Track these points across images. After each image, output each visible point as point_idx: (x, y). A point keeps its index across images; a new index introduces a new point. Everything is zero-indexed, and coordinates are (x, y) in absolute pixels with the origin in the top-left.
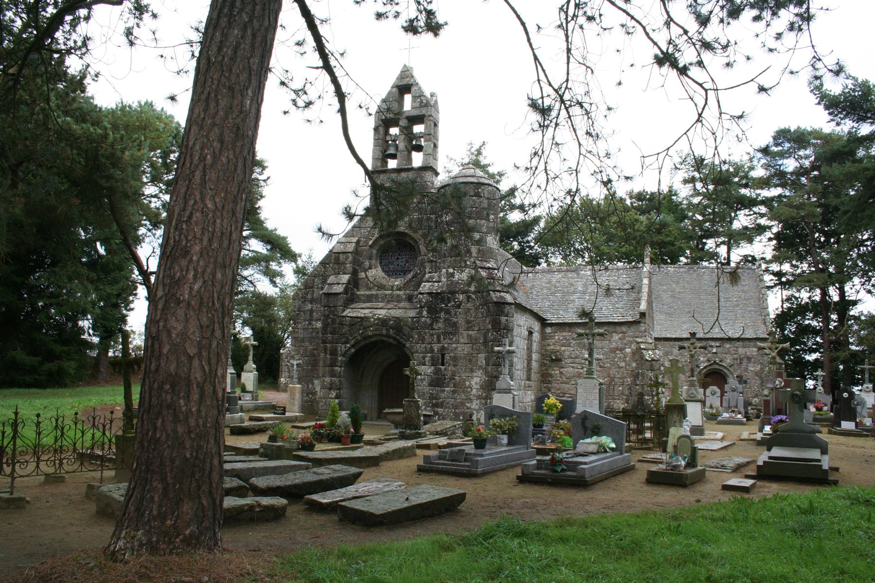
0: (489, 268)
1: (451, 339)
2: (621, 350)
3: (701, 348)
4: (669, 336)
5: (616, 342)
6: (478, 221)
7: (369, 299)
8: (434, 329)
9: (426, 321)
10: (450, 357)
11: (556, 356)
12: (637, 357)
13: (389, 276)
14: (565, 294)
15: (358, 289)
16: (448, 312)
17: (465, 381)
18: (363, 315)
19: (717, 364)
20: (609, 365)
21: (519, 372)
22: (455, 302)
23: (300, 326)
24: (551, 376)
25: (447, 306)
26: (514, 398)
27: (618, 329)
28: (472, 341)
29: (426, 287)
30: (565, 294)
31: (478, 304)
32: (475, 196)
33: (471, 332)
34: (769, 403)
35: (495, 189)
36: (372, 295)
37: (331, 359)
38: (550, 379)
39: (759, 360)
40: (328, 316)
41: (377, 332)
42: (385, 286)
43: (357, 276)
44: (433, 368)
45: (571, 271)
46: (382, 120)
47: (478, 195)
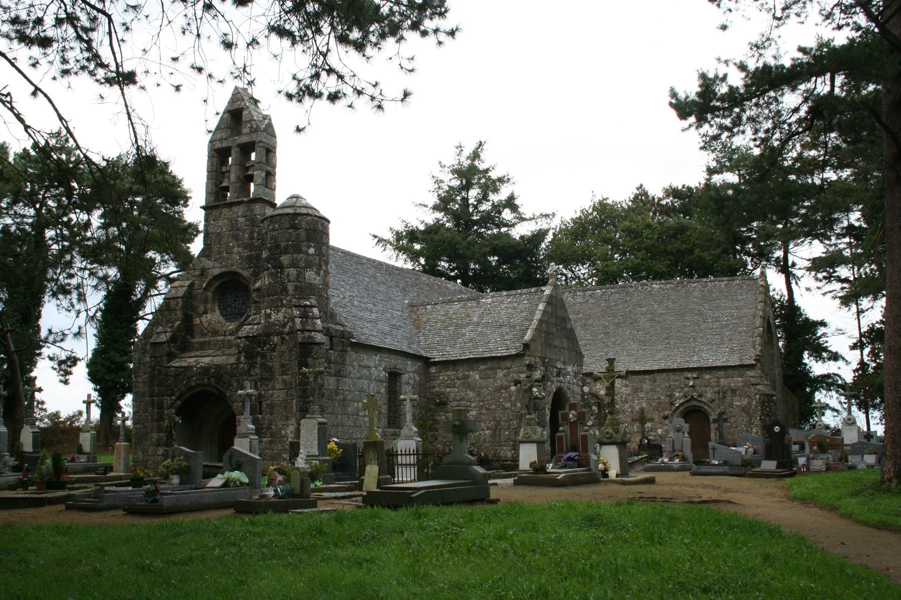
0: (306, 306)
1: (267, 386)
2: (507, 388)
4: (637, 368)
6: (295, 255)
7: (203, 346)
8: (252, 376)
9: (243, 367)
11: (440, 399)
13: (227, 320)
14: (459, 326)
15: (193, 337)
16: (264, 356)
18: (186, 365)
19: (696, 400)
20: (494, 407)
22: (270, 345)
23: (140, 379)
26: (250, 442)
28: (287, 386)
30: (459, 326)
32: (291, 228)
33: (285, 377)
34: (562, 441)
35: (316, 219)
38: (437, 426)
39: (746, 393)
40: (155, 367)
41: (200, 382)
42: (218, 332)
43: (191, 321)
45: (471, 300)
46: (216, 150)
47: (295, 227)
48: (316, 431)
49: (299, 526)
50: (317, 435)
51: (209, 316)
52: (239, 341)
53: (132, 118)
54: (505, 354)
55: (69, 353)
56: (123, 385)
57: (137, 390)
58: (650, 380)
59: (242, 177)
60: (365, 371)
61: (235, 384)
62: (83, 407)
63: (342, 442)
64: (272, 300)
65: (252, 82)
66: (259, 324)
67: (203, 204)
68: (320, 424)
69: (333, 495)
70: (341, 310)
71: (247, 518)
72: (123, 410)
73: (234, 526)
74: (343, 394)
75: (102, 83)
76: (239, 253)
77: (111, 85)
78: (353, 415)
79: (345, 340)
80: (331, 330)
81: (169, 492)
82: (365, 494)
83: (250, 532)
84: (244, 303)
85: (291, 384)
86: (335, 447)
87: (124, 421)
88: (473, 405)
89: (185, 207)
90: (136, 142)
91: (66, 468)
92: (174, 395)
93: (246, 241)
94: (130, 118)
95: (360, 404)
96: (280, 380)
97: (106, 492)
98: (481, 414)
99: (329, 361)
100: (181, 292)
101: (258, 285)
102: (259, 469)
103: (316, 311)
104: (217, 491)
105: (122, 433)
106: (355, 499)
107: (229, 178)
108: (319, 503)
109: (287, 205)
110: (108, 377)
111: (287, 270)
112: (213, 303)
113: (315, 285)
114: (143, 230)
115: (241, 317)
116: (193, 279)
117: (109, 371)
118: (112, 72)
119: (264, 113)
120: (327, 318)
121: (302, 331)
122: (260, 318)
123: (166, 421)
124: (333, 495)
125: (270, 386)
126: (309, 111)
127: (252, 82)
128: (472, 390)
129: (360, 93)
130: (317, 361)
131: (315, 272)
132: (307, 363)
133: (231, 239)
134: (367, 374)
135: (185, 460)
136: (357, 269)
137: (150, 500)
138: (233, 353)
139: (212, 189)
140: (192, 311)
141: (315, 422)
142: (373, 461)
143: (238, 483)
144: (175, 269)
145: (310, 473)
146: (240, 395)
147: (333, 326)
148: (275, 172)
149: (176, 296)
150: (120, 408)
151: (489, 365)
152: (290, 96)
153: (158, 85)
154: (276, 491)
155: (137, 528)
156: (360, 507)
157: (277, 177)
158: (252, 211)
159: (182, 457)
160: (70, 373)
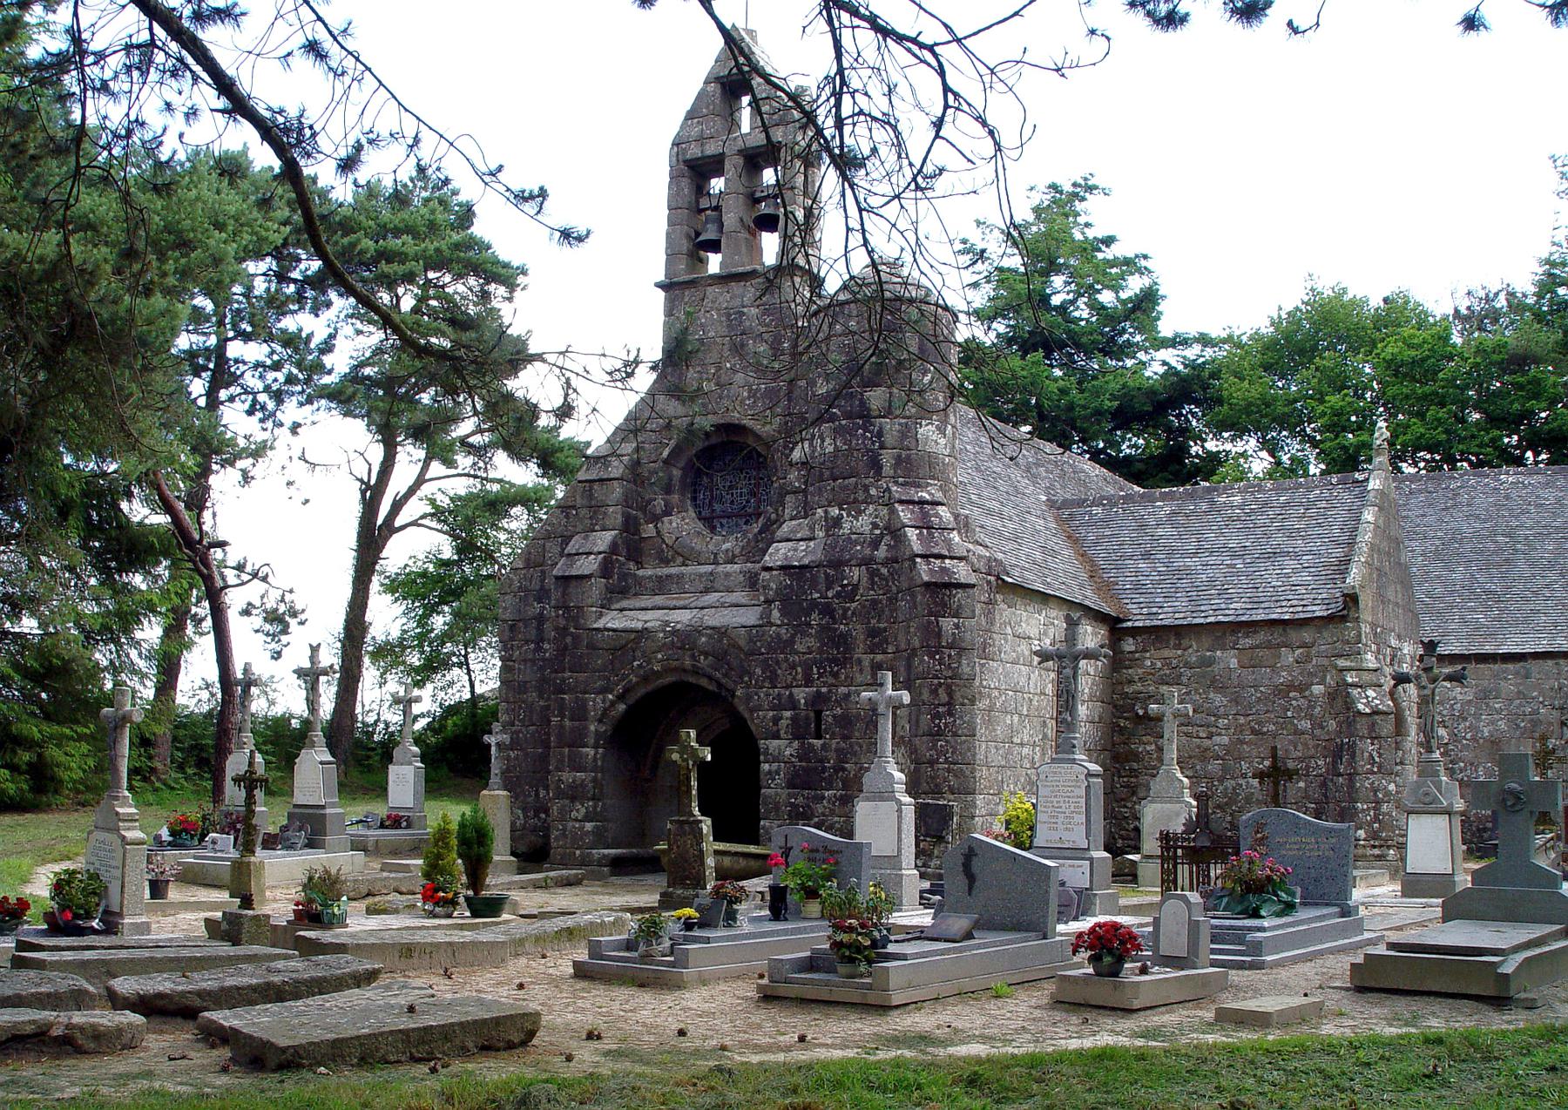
0: (922, 502)
1: (836, 675)
2: (1302, 688)
3: (1449, 678)
5: (1288, 668)
7: (661, 586)
8: (797, 653)
9: (778, 635)
12: (1339, 703)
18: (640, 625)
20: (1272, 727)
21: (1025, 751)
24: (1136, 756)
27: (1294, 636)
29: (779, 553)
38: (1135, 766)
40: (565, 629)
43: (637, 532)
44: (796, 744)
54: (1302, 616)
58: (1517, 674)
61: (758, 671)
64: (844, 488)
67: (661, 277)
74: (989, 696)
88: (1222, 722)
96: (866, 663)
98: (1242, 742)
128: (1221, 689)
151: (1262, 636)
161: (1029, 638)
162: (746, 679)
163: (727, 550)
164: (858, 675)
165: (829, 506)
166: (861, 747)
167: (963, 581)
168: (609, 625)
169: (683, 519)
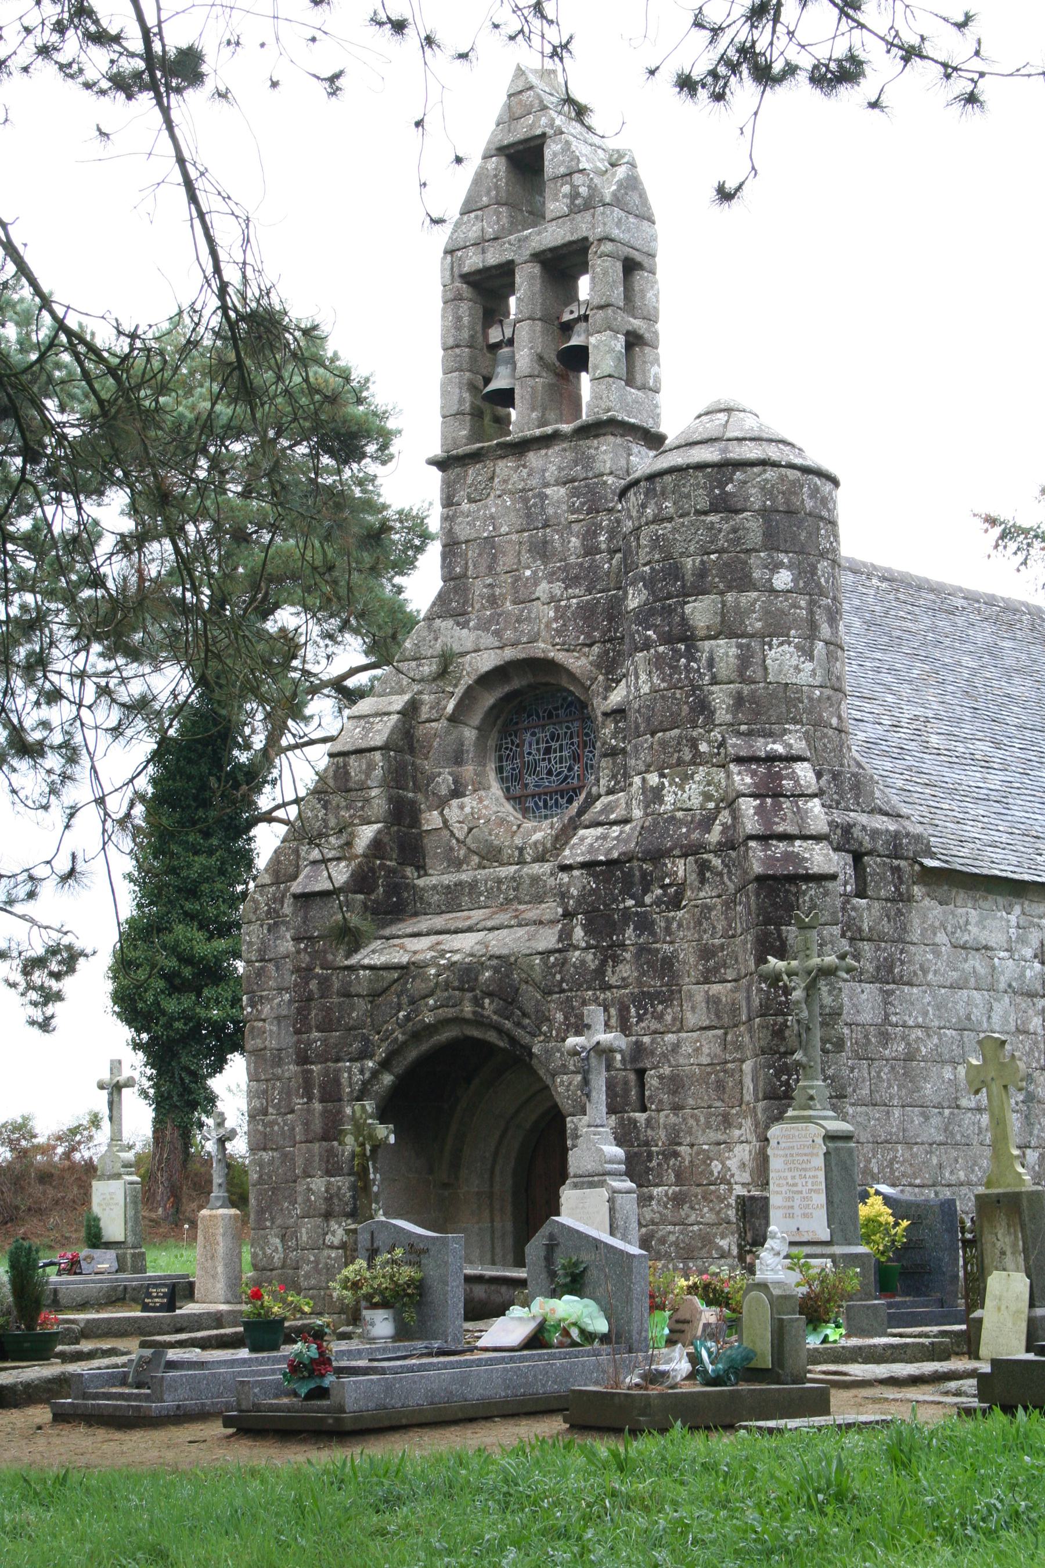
0: (772, 758)
1: (660, 1017)
6: (730, 597)
8: (610, 987)
9: (583, 962)
10: (661, 1077)
13: (525, 812)
15: (422, 869)
16: (645, 924)
17: (708, 1159)
18: (405, 959)
22: (664, 887)
23: (266, 1010)
25: (640, 903)
26: (611, 1201)
31: (731, 886)
32: (714, 509)
33: (716, 989)
35: (796, 474)
36: (459, 884)
37: (325, 1113)
40: (309, 969)
41: (450, 1012)
43: (416, 822)
46: (466, 278)
47: (724, 506)
48: (820, 1162)
49: (772, 1476)
50: (821, 1175)
51: (469, 802)
52: (565, 877)
53: (201, 196)
55: (55, 935)
56: (217, 1028)
57: (258, 1043)
59: (552, 357)
60: (975, 963)
61: (559, 1016)
62: (100, 1101)
63: (909, 1195)
64: (663, 744)
65: (565, 46)
66: (626, 821)
67: (436, 450)
68: (830, 1137)
69: (882, 1370)
70: (888, 765)
71: (603, 1447)
72: (220, 1106)
73: (564, 1474)
75: (103, 92)
76: (553, 599)
77: (130, 97)
78: (940, 1106)
79: (903, 863)
80: (856, 832)
81: (362, 1363)
82: (986, 1368)
83: (614, 1494)
84: (576, 758)
85: (734, 1011)
86: (886, 1215)
87: (222, 1142)
89: (384, 463)
90: (217, 270)
91: (55, 1292)
92: (371, 1057)
93: (572, 560)
94: (193, 198)
95: (962, 1070)
96: (699, 998)
97: (172, 1365)
99: (854, 934)
100: (381, 732)
101: (616, 697)
102: (639, 1289)
103: (804, 772)
104: (512, 1359)
105: (217, 1179)
106: (953, 1385)
107: (512, 361)
108: (837, 1397)
109: (697, 437)
110: (171, 1006)
111: (707, 645)
112: (481, 760)
113: (798, 688)
114: (257, 542)
115: (570, 801)
116: (416, 687)
117: (175, 984)
118: (133, 55)
119: (611, 144)
120: (841, 794)
121: (764, 838)
122: (628, 805)
123: (349, 1139)
124: (882, 1370)
125: (668, 1018)
126: (748, 130)
127: (565, 46)
129: (911, 54)
130: (814, 933)
131: (798, 647)
132: (783, 943)
133: (525, 557)
134: (982, 971)
135: (410, 1263)
136: (933, 629)
137: (303, 1392)
138: (546, 917)
139: (461, 401)
140: (417, 789)
141: (815, 1132)
142: (1009, 1260)
143: (575, 1333)
144: (364, 660)
145: (807, 1297)
146: (575, 1053)
147: (863, 819)
148: (656, 334)
149: (364, 745)
150: (211, 1099)
152: (686, 84)
153: (274, 84)
154: (694, 1359)
155: (263, 1482)
156: (969, 1412)
157: (663, 350)
158: (587, 461)
159: (399, 1252)
160: (58, 997)
161: (991, 949)
162: (545, 1028)
163: (535, 843)
164: (689, 1015)
165: (647, 771)
166: (698, 1121)
167: (815, 870)
168: (366, 961)
169: (481, 800)
